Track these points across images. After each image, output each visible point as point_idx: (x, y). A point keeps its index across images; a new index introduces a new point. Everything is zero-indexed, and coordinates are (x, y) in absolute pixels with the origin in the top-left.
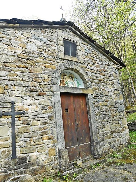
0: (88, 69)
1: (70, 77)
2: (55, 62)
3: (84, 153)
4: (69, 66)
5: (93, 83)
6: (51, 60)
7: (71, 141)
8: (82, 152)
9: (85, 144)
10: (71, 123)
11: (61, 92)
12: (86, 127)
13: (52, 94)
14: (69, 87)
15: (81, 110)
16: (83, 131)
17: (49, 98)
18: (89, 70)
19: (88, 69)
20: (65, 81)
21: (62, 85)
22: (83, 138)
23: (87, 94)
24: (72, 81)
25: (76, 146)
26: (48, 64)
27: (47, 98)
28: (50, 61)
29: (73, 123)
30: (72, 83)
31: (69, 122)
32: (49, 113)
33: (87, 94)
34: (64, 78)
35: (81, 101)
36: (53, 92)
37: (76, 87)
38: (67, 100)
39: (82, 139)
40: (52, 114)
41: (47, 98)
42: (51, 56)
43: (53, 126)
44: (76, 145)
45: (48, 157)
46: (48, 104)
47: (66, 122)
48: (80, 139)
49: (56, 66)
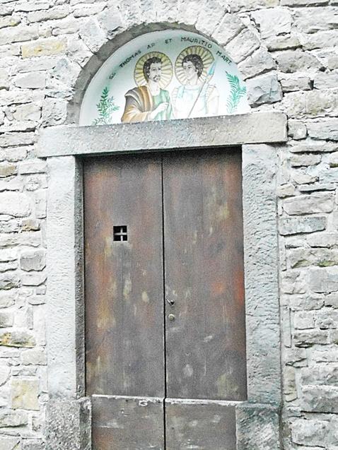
1: (184, 60)
2: (71, 18)
3: (193, 443)
6: (47, 16)
7: (128, 373)
8: (181, 435)
9: (205, 402)
10: (135, 294)
12: (226, 321)
13: (41, 165)
15: (202, 230)
16: (202, 338)
17: (29, 187)
21: (134, 112)
22: (197, 366)
25: (149, 399)
27: (21, 188)
28: (46, 20)
29: (149, 294)
30: (196, 94)
31: (127, 288)
32: (27, 245)
34: (147, 78)
35: (211, 176)
38: (103, 179)
39: (196, 375)
40: (36, 250)
41: (21, 188)
43: (35, 295)
44: (152, 395)
45: (9, 407)
46: (21, 212)
47: (114, 286)
48: (182, 374)
49: (70, 37)
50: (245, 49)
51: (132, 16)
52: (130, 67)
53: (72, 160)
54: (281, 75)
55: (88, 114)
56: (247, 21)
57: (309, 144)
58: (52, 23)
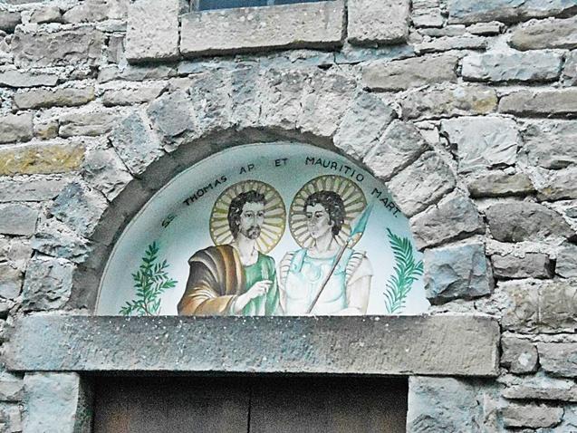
0: (487, 82)
1: (312, 199)
2: (95, 107)
4: (213, 111)
5: (528, 246)
6: (52, 98)
11: (90, 366)
14: (157, 318)
18: (488, 92)
19: (487, 82)
20: (246, 252)
23: (397, 386)
24: (327, 247)
26: (25, 140)
28: (49, 106)
30: (326, 269)
33: (397, 386)
34: (235, 230)
36: (20, 374)
37: (378, 308)
42: (59, 62)
50: (424, 191)
51: (213, 111)
52: (204, 207)
53: (73, 381)
54: (494, 246)
55: (113, 297)
56: (432, 137)
57: (543, 384)
58: (60, 113)
